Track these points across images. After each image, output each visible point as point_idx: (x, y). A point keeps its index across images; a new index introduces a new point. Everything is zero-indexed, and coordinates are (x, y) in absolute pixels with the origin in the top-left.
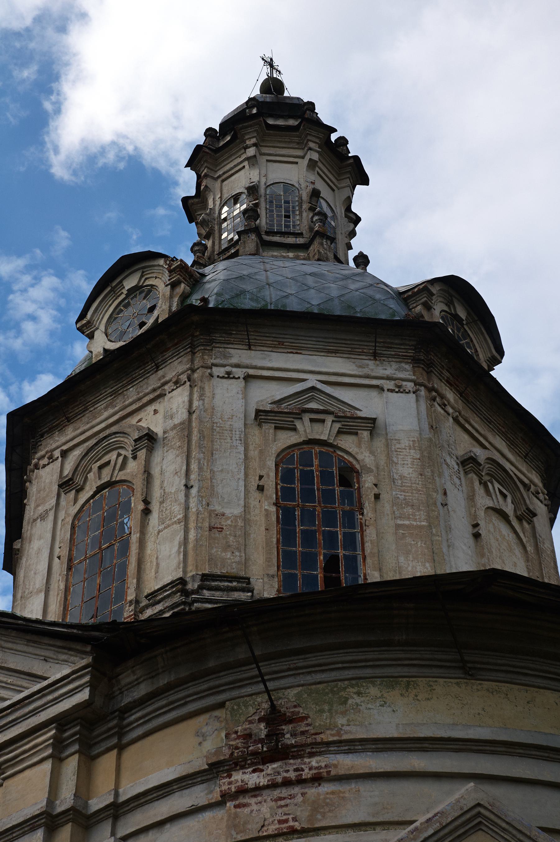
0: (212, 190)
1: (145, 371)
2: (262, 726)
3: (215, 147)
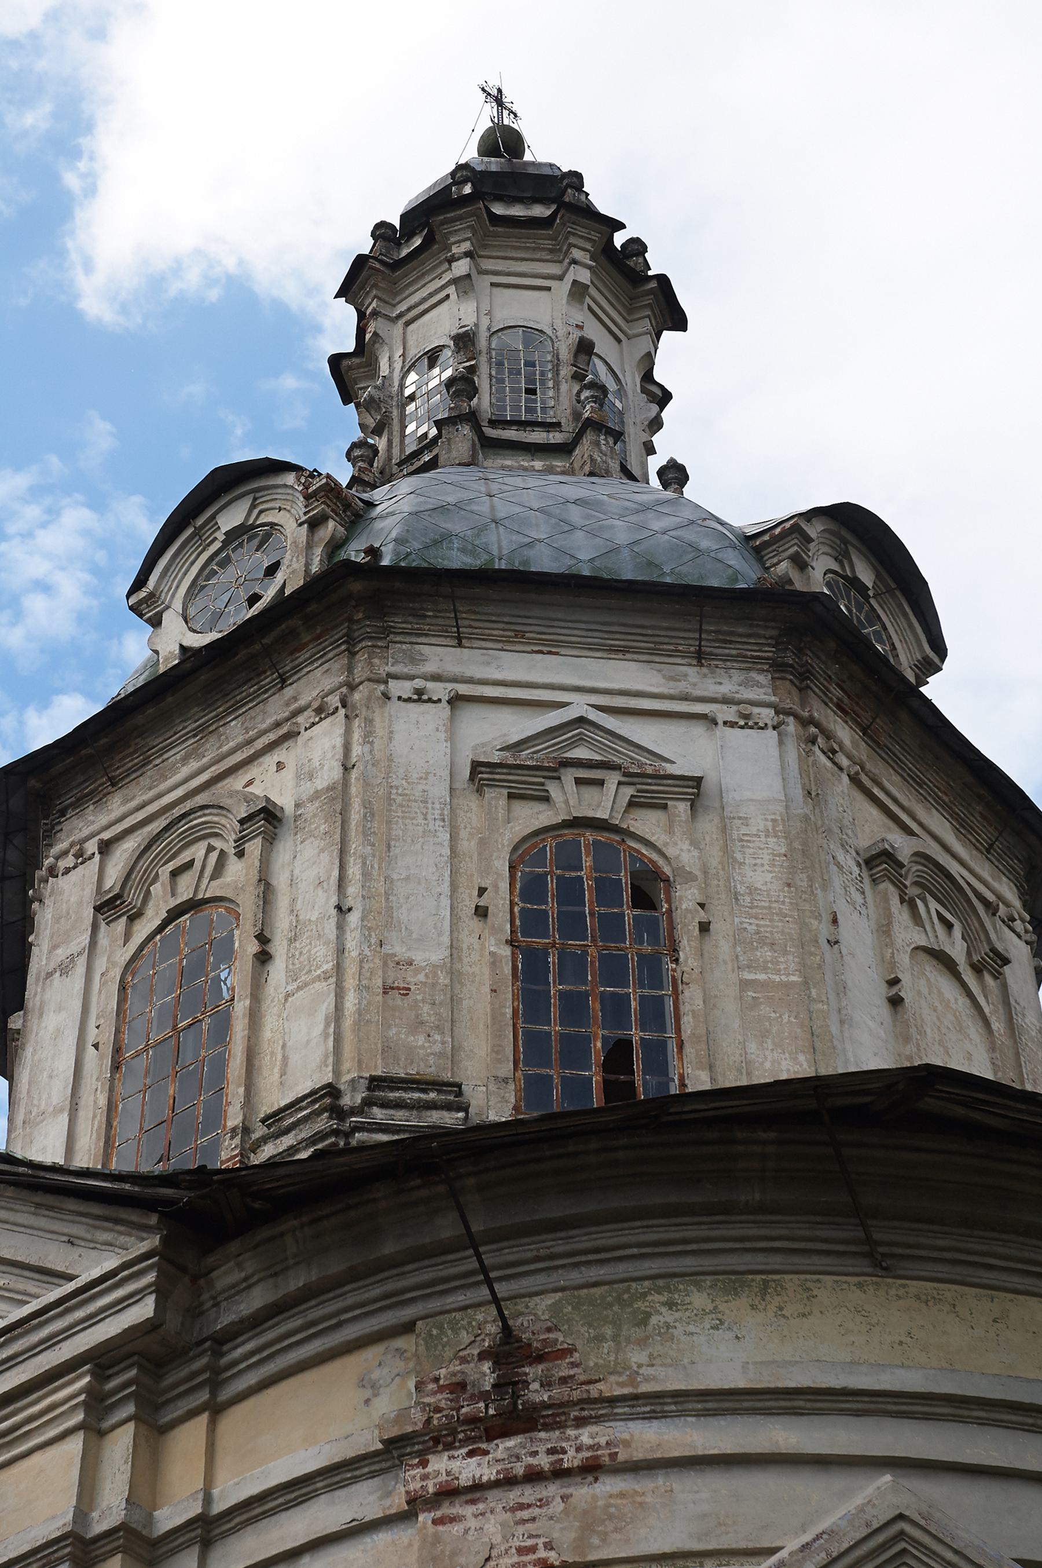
0: (387, 341)
1: (259, 689)
2: (486, 1366)
3: (392, 259)
